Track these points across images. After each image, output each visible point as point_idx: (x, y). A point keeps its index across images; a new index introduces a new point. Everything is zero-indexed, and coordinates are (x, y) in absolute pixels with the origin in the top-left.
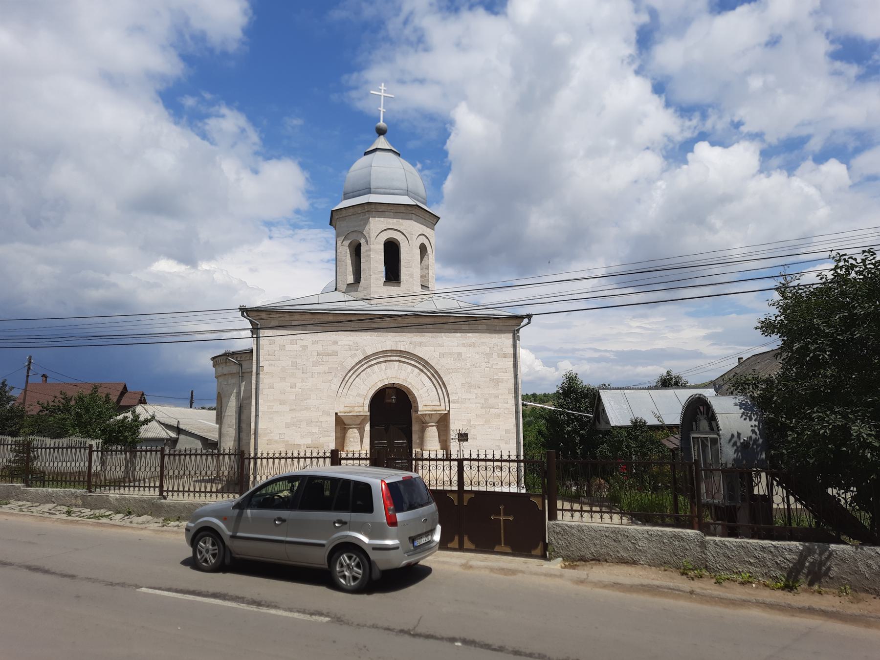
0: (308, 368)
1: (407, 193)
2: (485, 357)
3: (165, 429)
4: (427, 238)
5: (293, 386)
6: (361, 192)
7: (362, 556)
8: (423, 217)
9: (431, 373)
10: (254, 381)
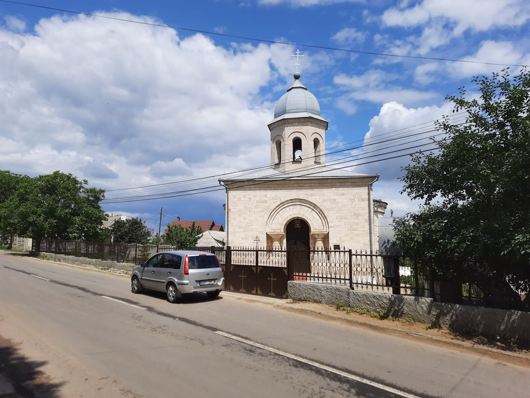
0: (252, 210)
1: (306, 110)
2: (350, 201)
3: (217, 243)
4: (319, 135)
5: (245, 219)
6: (282, 113)
7: (175, 287)
8: (316, 123)
9: (318, 211)
10: (226, 216)
